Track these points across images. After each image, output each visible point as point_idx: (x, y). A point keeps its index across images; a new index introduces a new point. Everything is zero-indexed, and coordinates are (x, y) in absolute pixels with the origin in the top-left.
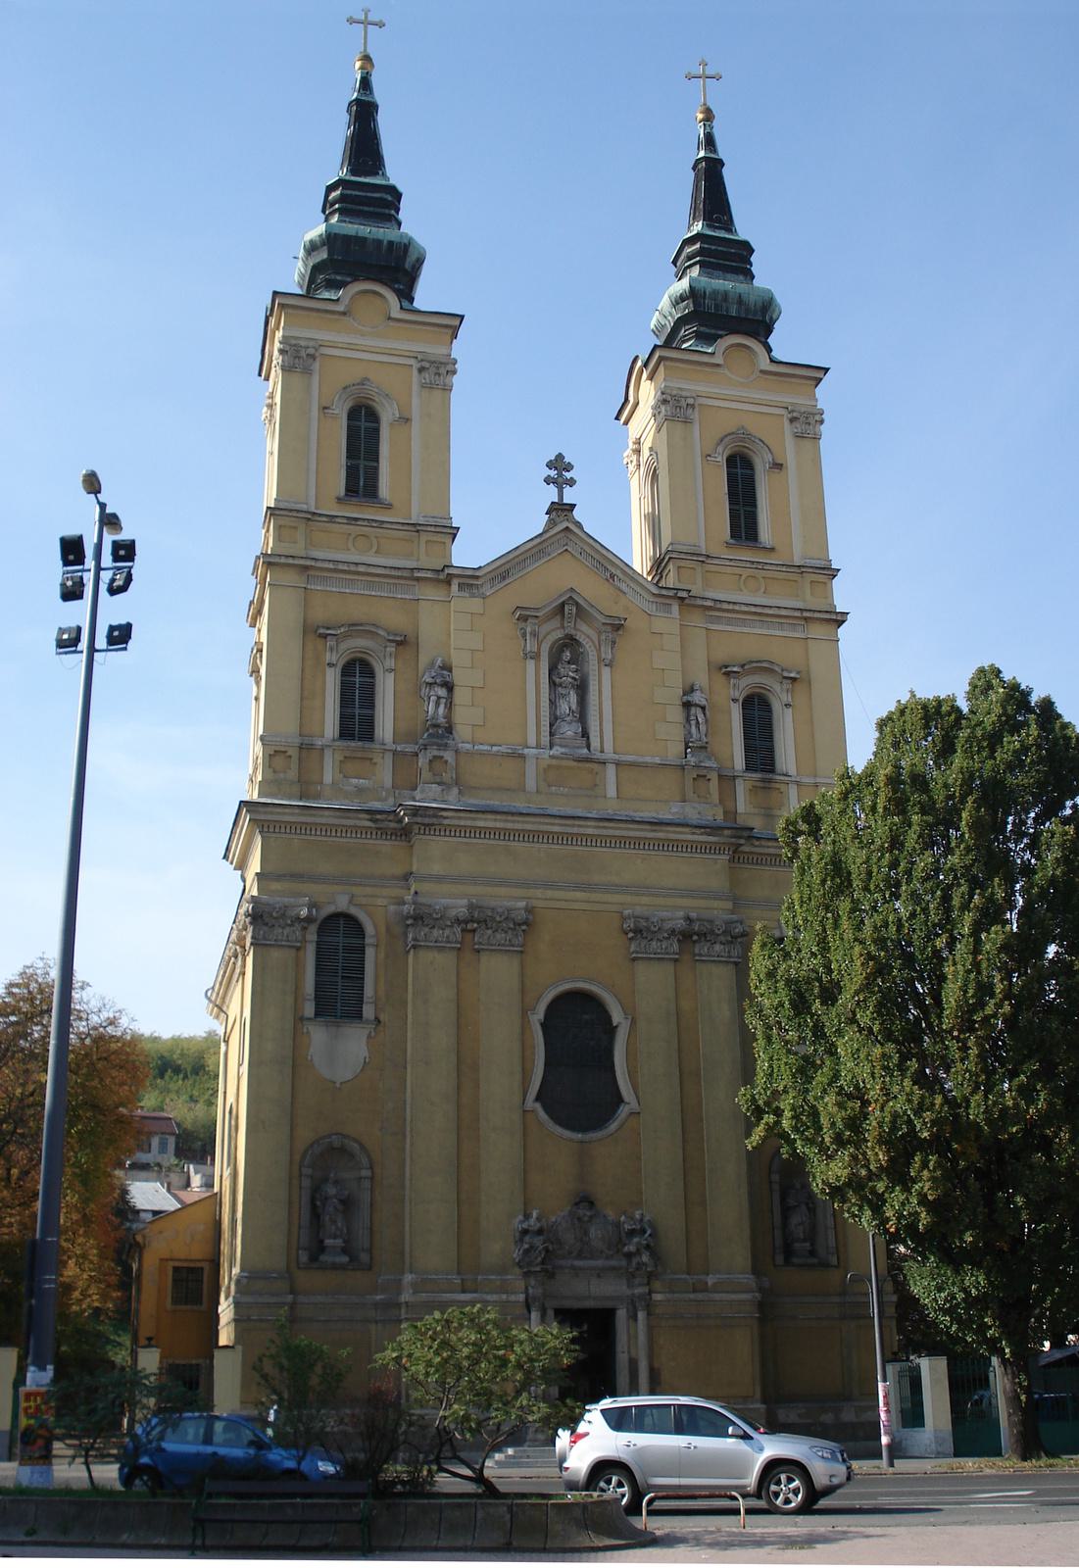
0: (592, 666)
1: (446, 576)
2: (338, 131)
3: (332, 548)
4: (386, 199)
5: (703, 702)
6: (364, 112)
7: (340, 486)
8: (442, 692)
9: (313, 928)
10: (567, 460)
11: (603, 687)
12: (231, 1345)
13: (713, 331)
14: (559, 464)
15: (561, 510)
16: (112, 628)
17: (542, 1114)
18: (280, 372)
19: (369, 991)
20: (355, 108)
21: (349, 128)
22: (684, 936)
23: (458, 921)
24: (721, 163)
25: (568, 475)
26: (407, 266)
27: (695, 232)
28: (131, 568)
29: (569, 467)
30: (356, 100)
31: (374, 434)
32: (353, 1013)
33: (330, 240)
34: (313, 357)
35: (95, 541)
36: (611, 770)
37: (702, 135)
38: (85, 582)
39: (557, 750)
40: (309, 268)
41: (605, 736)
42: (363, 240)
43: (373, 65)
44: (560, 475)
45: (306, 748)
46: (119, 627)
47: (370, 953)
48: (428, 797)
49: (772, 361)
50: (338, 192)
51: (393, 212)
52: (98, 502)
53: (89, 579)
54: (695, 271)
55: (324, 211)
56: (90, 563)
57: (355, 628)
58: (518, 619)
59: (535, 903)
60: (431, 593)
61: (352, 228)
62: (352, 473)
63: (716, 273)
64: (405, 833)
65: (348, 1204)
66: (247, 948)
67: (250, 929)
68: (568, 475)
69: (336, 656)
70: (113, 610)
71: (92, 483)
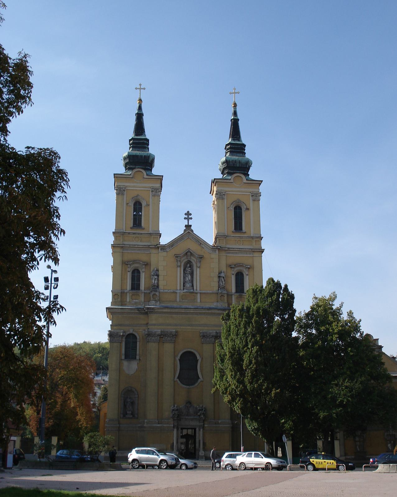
5: (224, 276)
7: (131, 224)
9: (124, 338)
10: (190, 213)
11: (197, 273)
14: (188, 214)
15: (188, 227)
16: (54, 296)
17: (179, 382)
19: (138, 352)
22: (216, 337)
25: (190, 217)
29: (191, 214)
30: (137, 113)
34: (225, 195)
39: (185, 291)
44: (188, 217)
47: (138, 343)
57: (134, 262)
60: (154, 251)
64: (146, 313)
65: (133, 403)
68: (190, 217)
69: (130, 269)
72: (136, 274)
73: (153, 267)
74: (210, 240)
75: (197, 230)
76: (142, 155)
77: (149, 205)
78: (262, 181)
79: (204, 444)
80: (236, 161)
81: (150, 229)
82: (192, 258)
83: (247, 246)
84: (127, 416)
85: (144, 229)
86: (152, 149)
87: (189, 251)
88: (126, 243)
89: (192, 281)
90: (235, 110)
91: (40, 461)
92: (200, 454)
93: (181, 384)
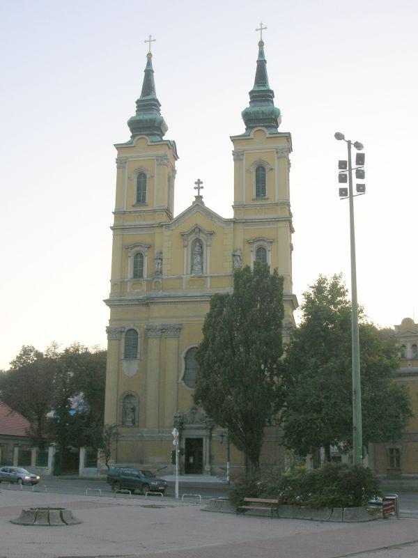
0: (205, 247)
3: (130, 222)
4: (56, 456)
5: (239, 254)
7: (134, 201)
8: (159, 261)
9: (124, 334)
14: (199, 182)
15: (199, 198)
17: (184, 384)
19: (139, 351)
24: (265, 61)
25: (201, 185)
29: (202, 183)
34: (126, 162)
36: (209, 279)
41: (208, 270)
45: (122, 282)
47: (139, 340)
48: (153, 294)
60: (158, 230)
64: (147, 304)
65: (133, 410)
68: (201, 185)
73: (157, 250)
74: (227, 213)
75: (209, 203)
77: (153, 177)
79: (211, 457)
80: (258, 113)
81: (277, 198)
82: (201, 234)
83: (270, 215)
84: (127, 424)
85: (147, 205)
86: (278, 103)
88: (126, 224)
89: (202, 264)
92: (205, 469)
93: (186, 387)
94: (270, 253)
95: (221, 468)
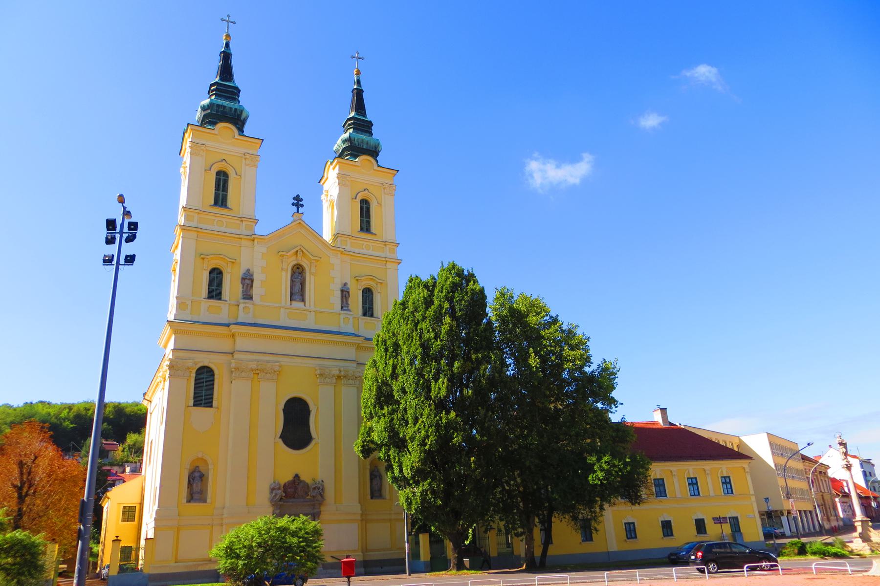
1: (252, 238)
2: (217, 63)
4: (234, 92)
6: (226, 57)
10: (301, 197)
12: (153, 537)
13: (357, 153)
16: (127, 256)
18: (189, 155)
20: (223, 54)
21: (220, 62)
22: (338, 377)
23: (252, 370)
24: (362, 91)
25: (301, 203)
26: (242, 118)
27: (352, 116)
28: (136, 233)
29: (301, 200)
30: (223, 51)
31: (226, 182)
32: (208, 403)
33: (211, 106)
35: (121, 222)
37: (356, 80)
38: (116, 237)
40: (203, 115)
42: (225, 107)
43: (230, 39)
44: (298, 202)
46: (130, 256)
49: (379, 166)
50: (215, 87)
51: (237, 97)
52: (123, 206)
53: (118, 236)
54: (351, 131)
55: (209, 93)
56: (118, 230)
58: (280, 256)
59: (282, 363)
61: (221, 102)
62: (216, 196)
63: (359, 132)
66: (166, 379)
67: (168, 371)
68: (301, 203)
70: (128, 249)
71: (121, 200)
72: (216, 276)
76: (231, 106)
78: (398, 171)
87: (300, 249)
90: (358, 78)
91: (475, 435)
94: (379, 295)
95: (332, 557)
